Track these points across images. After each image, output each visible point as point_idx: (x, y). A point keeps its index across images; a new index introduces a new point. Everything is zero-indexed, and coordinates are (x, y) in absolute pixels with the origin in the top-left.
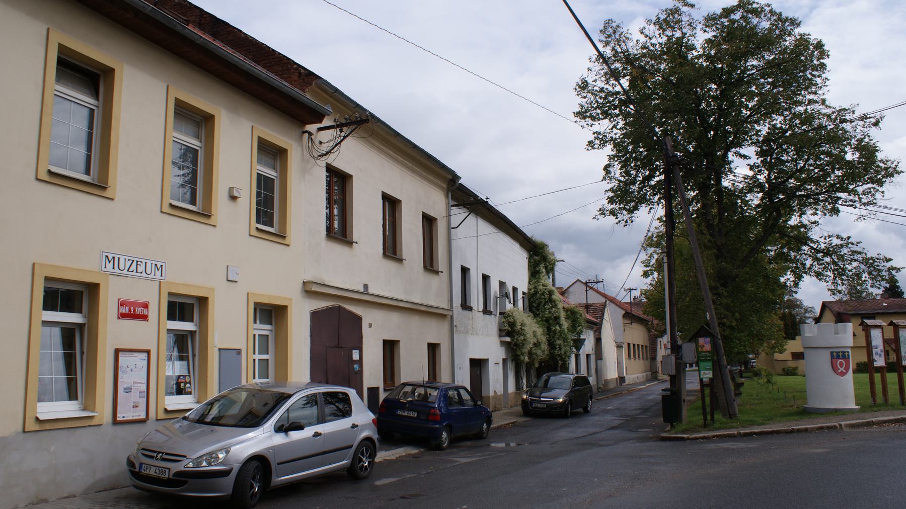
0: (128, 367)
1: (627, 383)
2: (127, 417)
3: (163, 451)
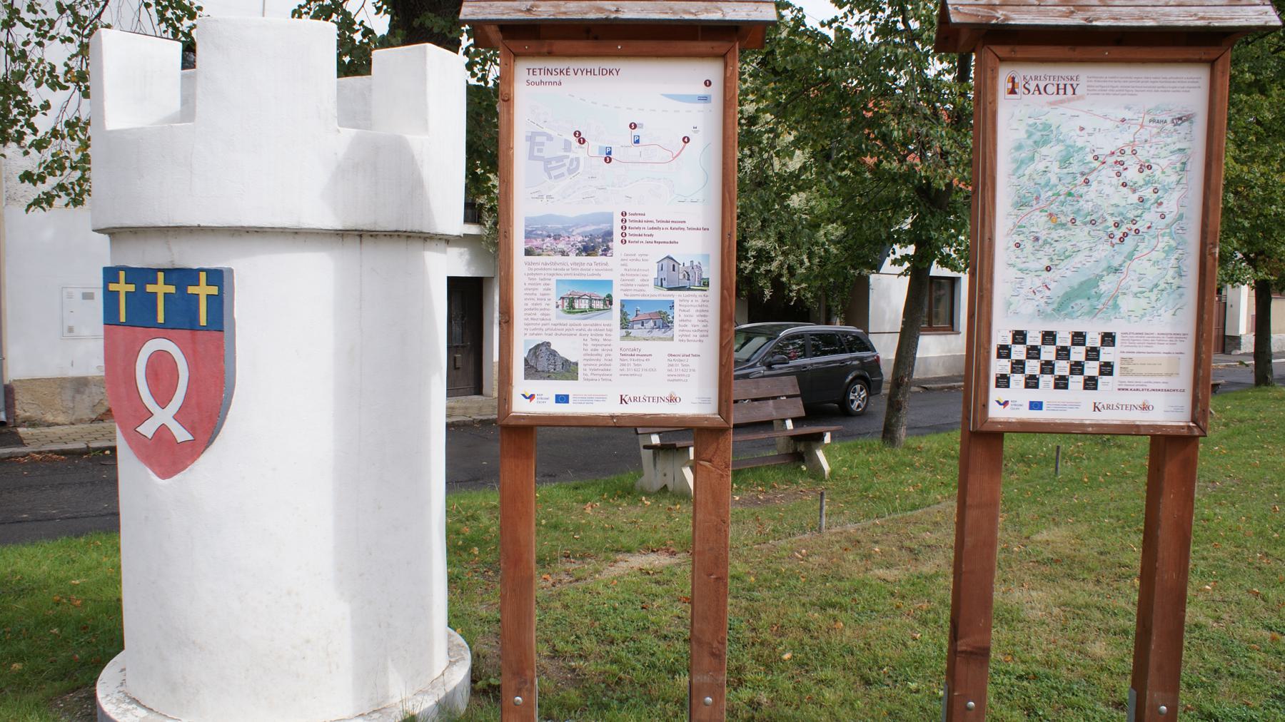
0: (582, 141)
1: (1242, 351)
2: (589, 399)
3: (94, 164)
